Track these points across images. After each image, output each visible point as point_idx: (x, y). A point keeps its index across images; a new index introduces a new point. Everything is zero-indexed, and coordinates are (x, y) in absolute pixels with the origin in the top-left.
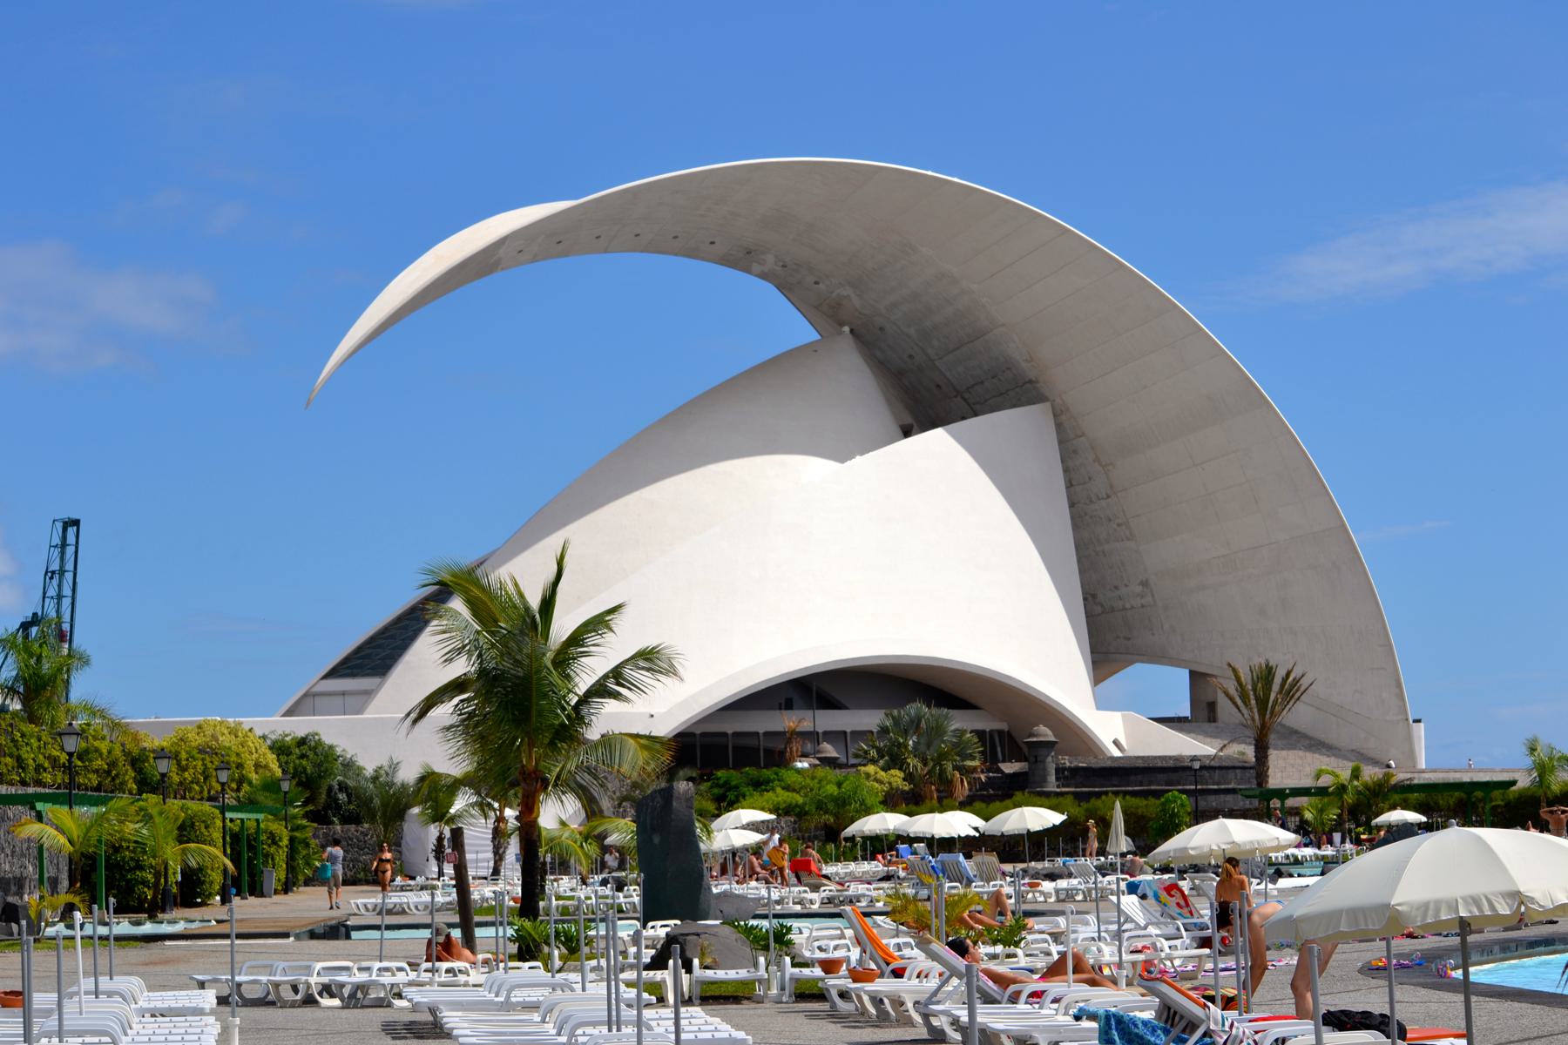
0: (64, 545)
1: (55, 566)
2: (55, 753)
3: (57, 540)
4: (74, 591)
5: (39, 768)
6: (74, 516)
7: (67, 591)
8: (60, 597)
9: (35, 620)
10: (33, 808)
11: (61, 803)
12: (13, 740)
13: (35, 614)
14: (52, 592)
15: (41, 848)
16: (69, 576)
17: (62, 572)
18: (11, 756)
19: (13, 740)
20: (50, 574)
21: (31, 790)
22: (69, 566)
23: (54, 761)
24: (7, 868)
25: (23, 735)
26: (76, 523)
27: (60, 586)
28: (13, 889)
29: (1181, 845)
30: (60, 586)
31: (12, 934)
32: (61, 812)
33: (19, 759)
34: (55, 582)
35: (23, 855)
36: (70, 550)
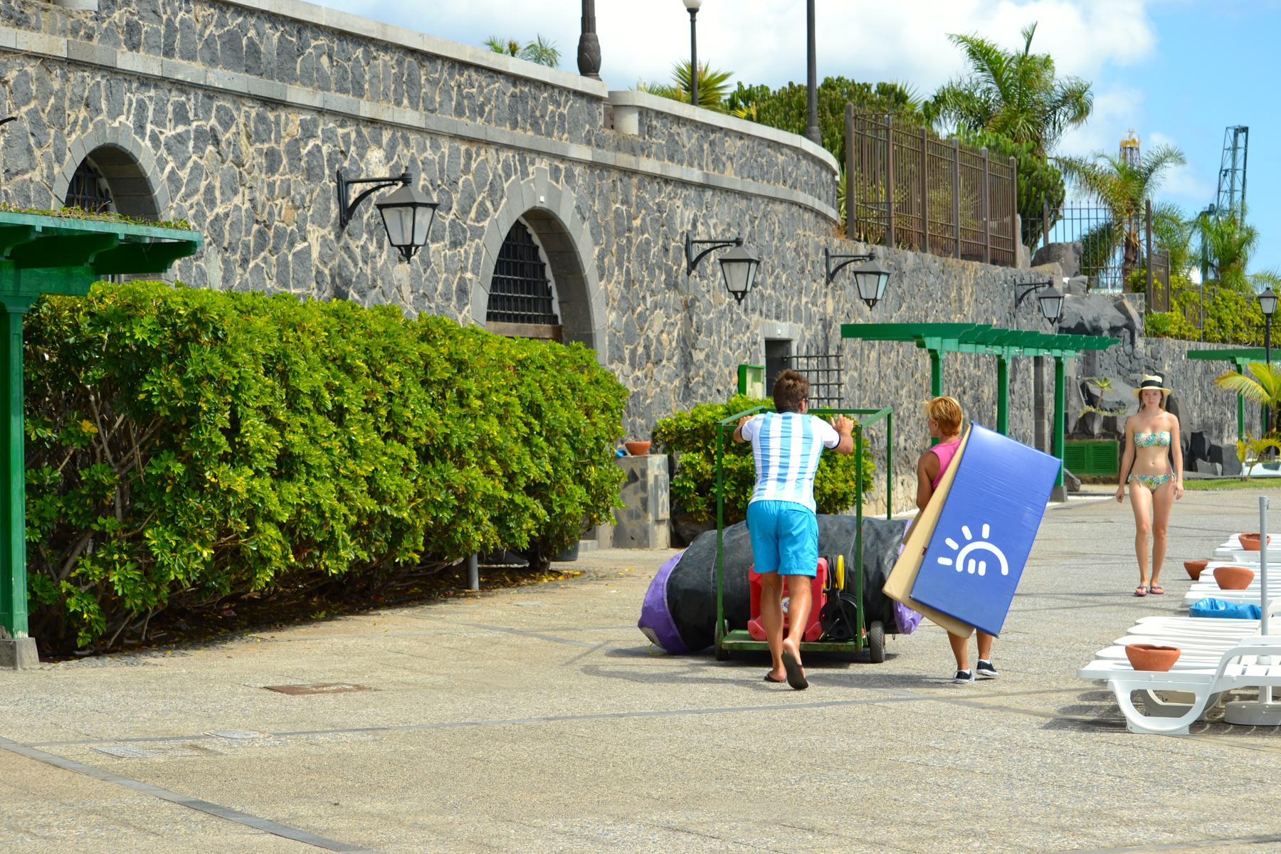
0: (1235, 148)
1: (1228, 166)
2: (1250, 315)
3: (1229, 144)
4: (1244, 185)
5: (1236, 328)
6: (1244, 124)
7: (1238, 186)
8: (1232, 191)
9: (1211, 211)
10: (1234, 362)
11: (1259, 358)
12: (1214, 304)
13: (1212, 205)
14: (1226, 187)
15: (1240, 398)
16: (1240, 174)
17: (1234, 170)
18: (1213, 317)
19: (1214, 304)
20: (1224, 172)
21: (1230, 347)
22: (1240, 165)
23: (1249, 322)
24: (1210, 414)
25: (1223, 299)
26: (1245, 130)
27: (1232, 182)
28: (1215, 432)
29: (27, 660)
30: (1232, 182)
31: (1216, 473)
32: (1257, 366)
33: (1220, 320)
34: (1228, 178)
35: (1223, 404)
36: (1240, 153)
